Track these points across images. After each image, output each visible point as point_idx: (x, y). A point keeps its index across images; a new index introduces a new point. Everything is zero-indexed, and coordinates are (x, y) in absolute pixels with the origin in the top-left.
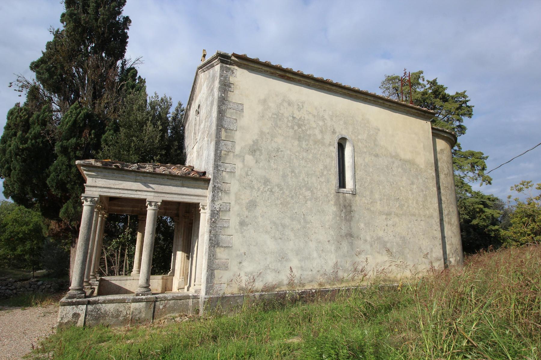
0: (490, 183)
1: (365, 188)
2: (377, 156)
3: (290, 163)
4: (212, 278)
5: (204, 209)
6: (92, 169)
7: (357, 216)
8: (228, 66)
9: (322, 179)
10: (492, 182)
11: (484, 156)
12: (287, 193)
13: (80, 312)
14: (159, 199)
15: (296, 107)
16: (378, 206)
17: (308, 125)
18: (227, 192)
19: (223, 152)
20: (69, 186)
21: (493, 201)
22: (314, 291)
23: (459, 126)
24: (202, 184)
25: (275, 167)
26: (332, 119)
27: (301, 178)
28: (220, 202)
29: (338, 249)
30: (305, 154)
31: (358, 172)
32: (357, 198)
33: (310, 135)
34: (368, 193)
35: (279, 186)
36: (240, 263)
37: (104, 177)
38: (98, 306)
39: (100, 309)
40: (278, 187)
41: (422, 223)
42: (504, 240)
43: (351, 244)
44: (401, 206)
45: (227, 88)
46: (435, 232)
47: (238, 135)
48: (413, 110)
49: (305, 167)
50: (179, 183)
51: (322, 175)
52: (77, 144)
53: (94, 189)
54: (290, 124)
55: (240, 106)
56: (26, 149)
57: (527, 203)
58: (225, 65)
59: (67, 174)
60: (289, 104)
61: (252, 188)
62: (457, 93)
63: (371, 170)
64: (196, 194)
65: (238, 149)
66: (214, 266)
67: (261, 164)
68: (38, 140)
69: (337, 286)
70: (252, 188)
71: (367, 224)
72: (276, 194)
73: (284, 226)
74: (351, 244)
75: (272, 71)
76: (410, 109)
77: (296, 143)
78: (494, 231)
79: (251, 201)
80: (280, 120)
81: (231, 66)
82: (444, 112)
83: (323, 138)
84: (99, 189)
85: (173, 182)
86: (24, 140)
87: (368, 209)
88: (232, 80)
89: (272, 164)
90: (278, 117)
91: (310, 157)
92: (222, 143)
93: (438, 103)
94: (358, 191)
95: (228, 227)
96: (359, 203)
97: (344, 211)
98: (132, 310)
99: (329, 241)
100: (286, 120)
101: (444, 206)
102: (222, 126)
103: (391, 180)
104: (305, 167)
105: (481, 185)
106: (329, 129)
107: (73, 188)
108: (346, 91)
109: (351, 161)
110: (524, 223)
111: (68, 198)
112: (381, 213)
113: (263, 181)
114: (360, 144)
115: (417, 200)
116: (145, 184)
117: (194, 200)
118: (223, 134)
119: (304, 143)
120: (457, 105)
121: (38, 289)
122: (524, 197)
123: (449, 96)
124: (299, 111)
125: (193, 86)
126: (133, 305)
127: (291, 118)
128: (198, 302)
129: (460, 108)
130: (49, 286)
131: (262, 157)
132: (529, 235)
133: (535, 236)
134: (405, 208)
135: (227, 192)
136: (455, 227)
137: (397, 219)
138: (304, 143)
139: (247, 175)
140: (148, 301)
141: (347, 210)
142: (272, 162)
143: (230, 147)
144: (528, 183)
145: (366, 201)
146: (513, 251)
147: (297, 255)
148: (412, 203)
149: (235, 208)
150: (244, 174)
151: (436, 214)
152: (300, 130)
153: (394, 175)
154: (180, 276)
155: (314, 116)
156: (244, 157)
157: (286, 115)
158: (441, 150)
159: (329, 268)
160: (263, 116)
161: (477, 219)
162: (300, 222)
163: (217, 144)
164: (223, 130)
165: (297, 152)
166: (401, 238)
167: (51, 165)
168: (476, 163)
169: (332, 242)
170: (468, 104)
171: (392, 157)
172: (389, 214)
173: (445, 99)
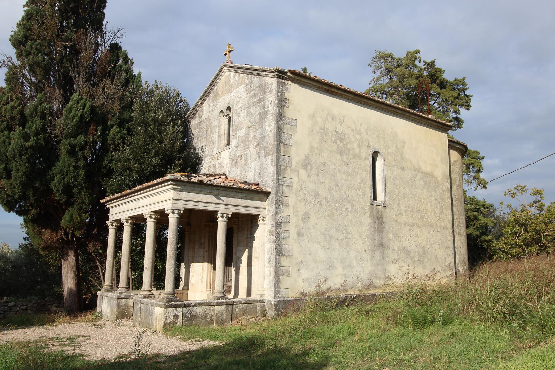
0: (485, 187)
1: (393, 200)
2: (403, 169)
3: (334, 177)
4: (278, 284)
5: (263, 220)
6: (178, 183)
7: (387, 227)
8: (283, 81)
9: (360, 192)
10: (487, 186)
11: (481, 155)
12: (333, 205)
13: (179, 314)
14: (229, 211)
15: (338, 121)
16: (404, 218)
17: (348, 140)
18: (286, 205)
19: (282, 167)
20: (75, 190)
21: (487, 208)
22: (355, 296)
23: (457, 119)
24: (262, 196)
25: (322, 180)
26: (367, 133)
27: (343, 191)
28: (282, 214)
29: (373, 257)
30: (346, 168)
31: (388, 185)
32: (387, 210)
33: (349, 149)
34: (396, 205)
35: (326, 199)
36: (299, 270)
37: (187, 191)
38: (191, 308)
39: (192, 312)
40: (326, 200)
41: (439, 234)
42: (495, 252)
43: (383, 253)
44: (422, 218)
45: (283, 103)
46: (449, 243)
47: (293, 150)
48: (434, 123)
49: (346, 180)
50: (244, 195)
51: (360, 188)
52: (86, 143)
53: (179, 202)
54: (333, 139)
55: (294, 121)
56: (31, 147)
57: (519, 210)
58: (281, 80)
59: (74, 177)
60: (333, 119)
61: (306, 201)
62: (456, 80)
63: (398, 183)
64: (257, 206)
65: (293, 164)
66: (280, 273)
67: (312, 178)
68: (39, 137)
69: (372, 292)
70: (306, 201)
71: (395, 235)
72: (324, 207)
73: (331, 237)
74: (383, 253)
75: (320, 85)
76: (432, 122)
77: (339, 157)
78: (487, 241)
79: (305, 213)
80: (326, 134)
81: (286, 82)
82: (440, 100)
83: (360, 152)
84: (183, 202)
85: (240, 195)
86: (26, 137)
87: (396, 221)
88: (287, 95)
89: (320, 178)
90: (324, 131)
91: (350, 170)
92: (282, 158)
93: (435, 89)
94: (388, 204)
95: (289, 238)
96: (389, 214)
97: (377, 222)
98: (215, 312)
99: (365, 251)
100: (330, 134)
101: (455, 217)
102: (281, 142)
103: (414, 193)
104: (346, 180)
105: (476, 189)
106: (365, 143)
107: (79, 193)
108: (379, 105)
109: (382, 174)
110: (516, 233)
111: (72, 204)
112: (406, 224)
113: (314, 195)
114: (389, 157)
115: (435, 212)
116: (217, 197)
117: (216, 209)
118: (282, 149)
119: (345, 156)
120: (455, 94)
121: (10, 311)
122: (517, 203)
123: (447, 82)
124: (341, 125)
125: (213, 82)
126: (217, 308)
127: (334, 133)
128: (264, 306)
129: (458, 97)
130: (25, 307)
131: (313, 171)
132: (520, 246)
133: (527, 248)
134: (425, 220)
135: (286, 205)
136: (463, 238)
137: (418, 230)
138: (345, 156)
139: (302, 189)
140: (227, 305)
141: (379, 221)
142: (320, 175)
143: (287, 162)
144: (523, 187)
145: (394, 213)
146: (503, 265)
147: (341, 263)
148: (431, 215)
149: (293, 220)
150: (299, 189)
151: (450, 225)
152: (342, 144)
153: (417, 188)
154: (207, 288)
155: (353, 130)
156: (298, 171)
157: (331, 129)
158: (455, 161)
159: (365, 277)
160: (312, 131)
161: (471, 229)
162: (343, 233)
163: (278, 158)
164: (282, 145)
165: (340, 166)
166: (421, 248)
167: (54, 165)
168: (473, 163)
169: (368, 251)
170: (467, 93)
171: (415, 170)
172: (412, 225)
173: (443, 85)
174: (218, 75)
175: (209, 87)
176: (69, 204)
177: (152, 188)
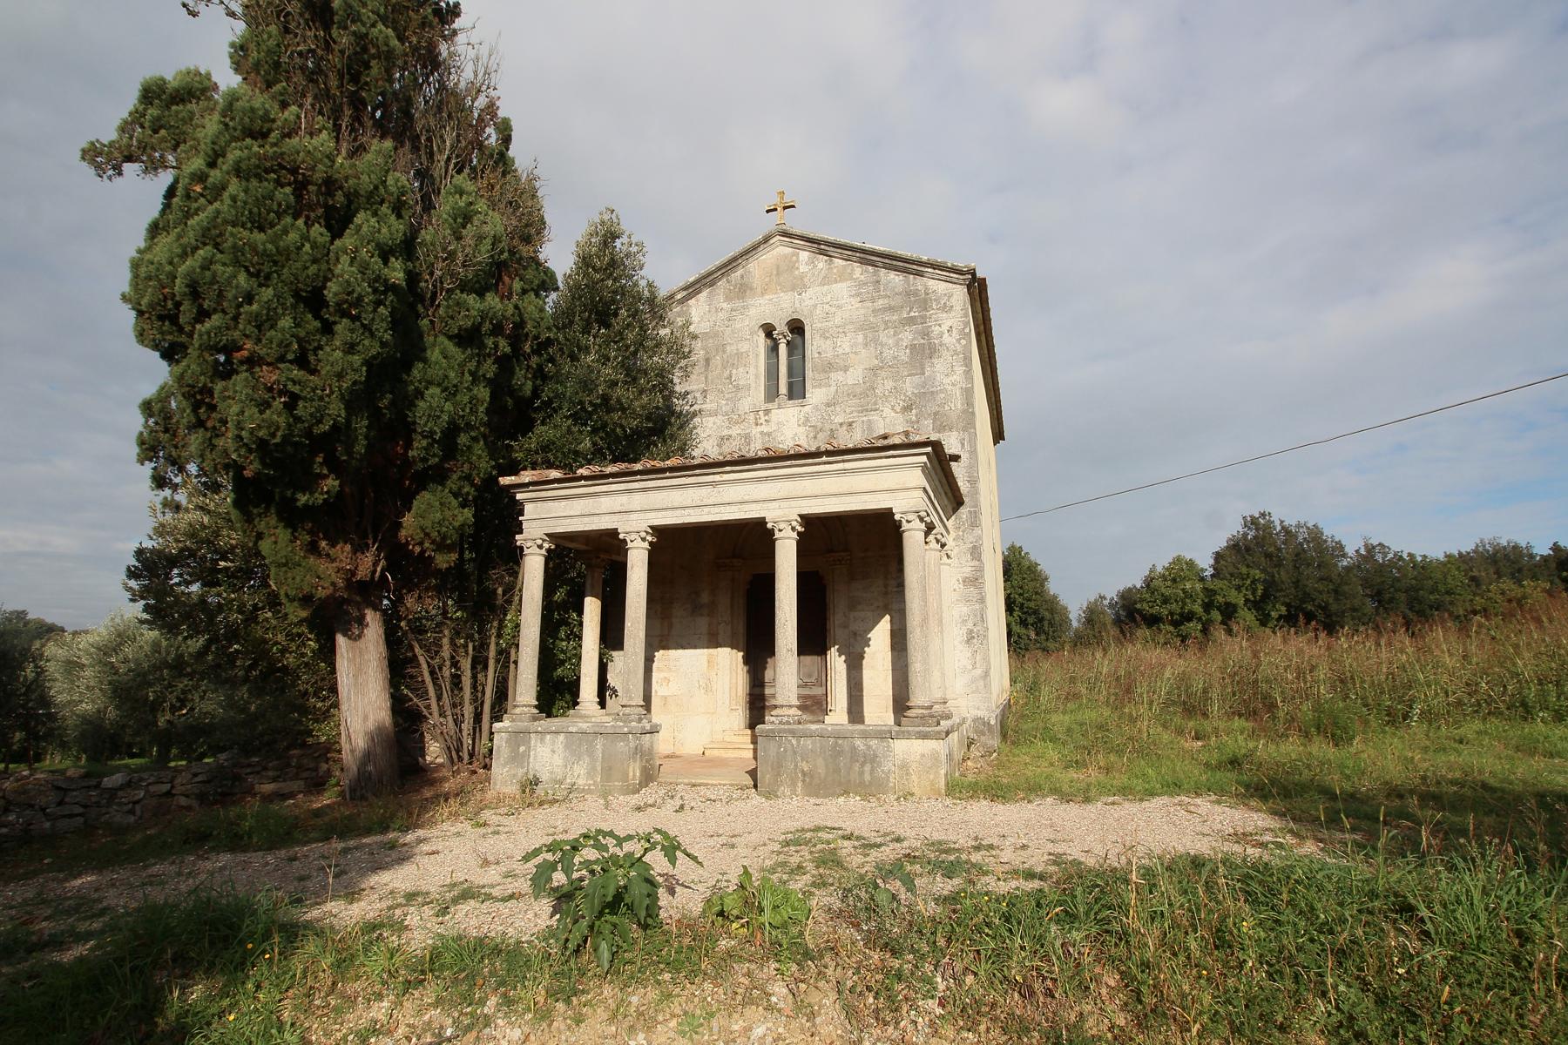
125: (735, 259)
130: (165, 788)
174: (754, 248)
175: (719, 269)
176: (438, 476)
177: (824, 459)
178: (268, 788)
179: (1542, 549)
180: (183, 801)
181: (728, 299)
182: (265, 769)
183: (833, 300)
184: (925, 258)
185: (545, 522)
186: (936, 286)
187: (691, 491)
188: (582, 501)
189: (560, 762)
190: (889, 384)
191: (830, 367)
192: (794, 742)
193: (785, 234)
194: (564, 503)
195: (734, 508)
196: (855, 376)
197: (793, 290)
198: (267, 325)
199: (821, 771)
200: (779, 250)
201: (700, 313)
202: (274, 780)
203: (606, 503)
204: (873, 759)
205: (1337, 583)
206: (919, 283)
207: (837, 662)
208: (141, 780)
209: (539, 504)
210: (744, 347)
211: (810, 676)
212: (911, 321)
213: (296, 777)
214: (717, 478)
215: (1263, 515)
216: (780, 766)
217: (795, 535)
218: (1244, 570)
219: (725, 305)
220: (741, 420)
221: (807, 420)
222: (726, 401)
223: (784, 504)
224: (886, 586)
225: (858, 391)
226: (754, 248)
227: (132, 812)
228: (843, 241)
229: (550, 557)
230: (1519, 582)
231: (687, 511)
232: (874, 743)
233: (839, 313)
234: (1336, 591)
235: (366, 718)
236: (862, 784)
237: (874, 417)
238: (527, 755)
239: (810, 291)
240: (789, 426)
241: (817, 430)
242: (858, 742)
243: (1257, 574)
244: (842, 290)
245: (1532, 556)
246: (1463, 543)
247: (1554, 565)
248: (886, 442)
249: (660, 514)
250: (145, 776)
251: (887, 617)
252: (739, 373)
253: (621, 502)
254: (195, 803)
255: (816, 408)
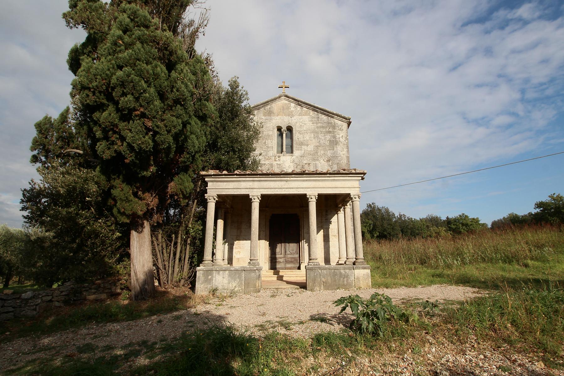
125: (268, 102)
174: (275, 99)
175: (262, 104)
178: (92, 297)
179: (444, 218)
180: (57, 304)
181: (264, 115)
182: (91, 289)
183: (303, 122)
184: (335, 112)
185: (217, 190)
186: (338, 122)
187: (278, 183)
188: (233, 183)
189: (227, 282)
190: (322, 152)
191: (302, 144)
192: (320, 271)
193: (287, 96)
194: (225, 183)
195: (294, 190)
196: (311, 148)
197: (289, 116)
198: (151, 103)
199: (329, 281)
200: (283, 102)
201: (257, 118)
202: (94, 293)
203: (243, 185)
204: (347, 276)
205: (393, 226)
206: (332, 120)
207: (305, 245)
208: (39, 294)
209: (215, 183)
210: (271, 133)
211: (293, 250)
212: (330, 132)
213: (103, 292)
214: (288, 179)
215: (373, 204)
216: (315, 280)
217: (259, 201)
218: (367, 221)
219: (263, 117)
220: (269, 159)
221: (294, 161)
222: (266, 152)
223: (312, 190)
224: (322, 220)
225: (312, 153)
226: (275, 99)
227: (35, 310)
228: (307, 102)
229: (217, 204)
230: (438, 227)
231: (276, 190)
232: (347, 271)
233: (305, 126)
234: (393, 228)
235: (144, 266)
236: (344, 285)
237: (317, 162)
238: (211, 280)
239: (295, 117)
240: (287, 163)
241: (297, 165)
242: (342, 271)
243: (371, 222)
244: (306, 118)
245: (441, 220)
246: (423, 215)
247: (446, 223)
248: (344, 172)
249: (266, 190)
250: (40, 292)
251: (322, 230)
252: (269, 142)
253: (305, 184)
254: (62, 305)
255: (297, 157)
